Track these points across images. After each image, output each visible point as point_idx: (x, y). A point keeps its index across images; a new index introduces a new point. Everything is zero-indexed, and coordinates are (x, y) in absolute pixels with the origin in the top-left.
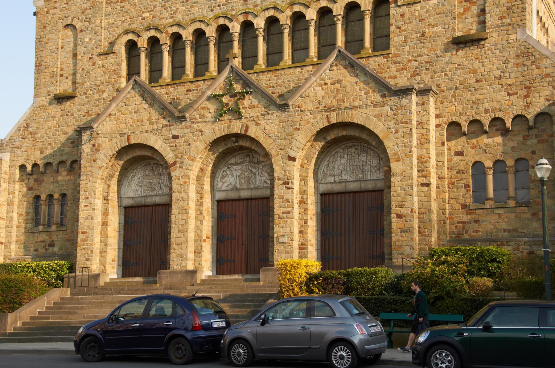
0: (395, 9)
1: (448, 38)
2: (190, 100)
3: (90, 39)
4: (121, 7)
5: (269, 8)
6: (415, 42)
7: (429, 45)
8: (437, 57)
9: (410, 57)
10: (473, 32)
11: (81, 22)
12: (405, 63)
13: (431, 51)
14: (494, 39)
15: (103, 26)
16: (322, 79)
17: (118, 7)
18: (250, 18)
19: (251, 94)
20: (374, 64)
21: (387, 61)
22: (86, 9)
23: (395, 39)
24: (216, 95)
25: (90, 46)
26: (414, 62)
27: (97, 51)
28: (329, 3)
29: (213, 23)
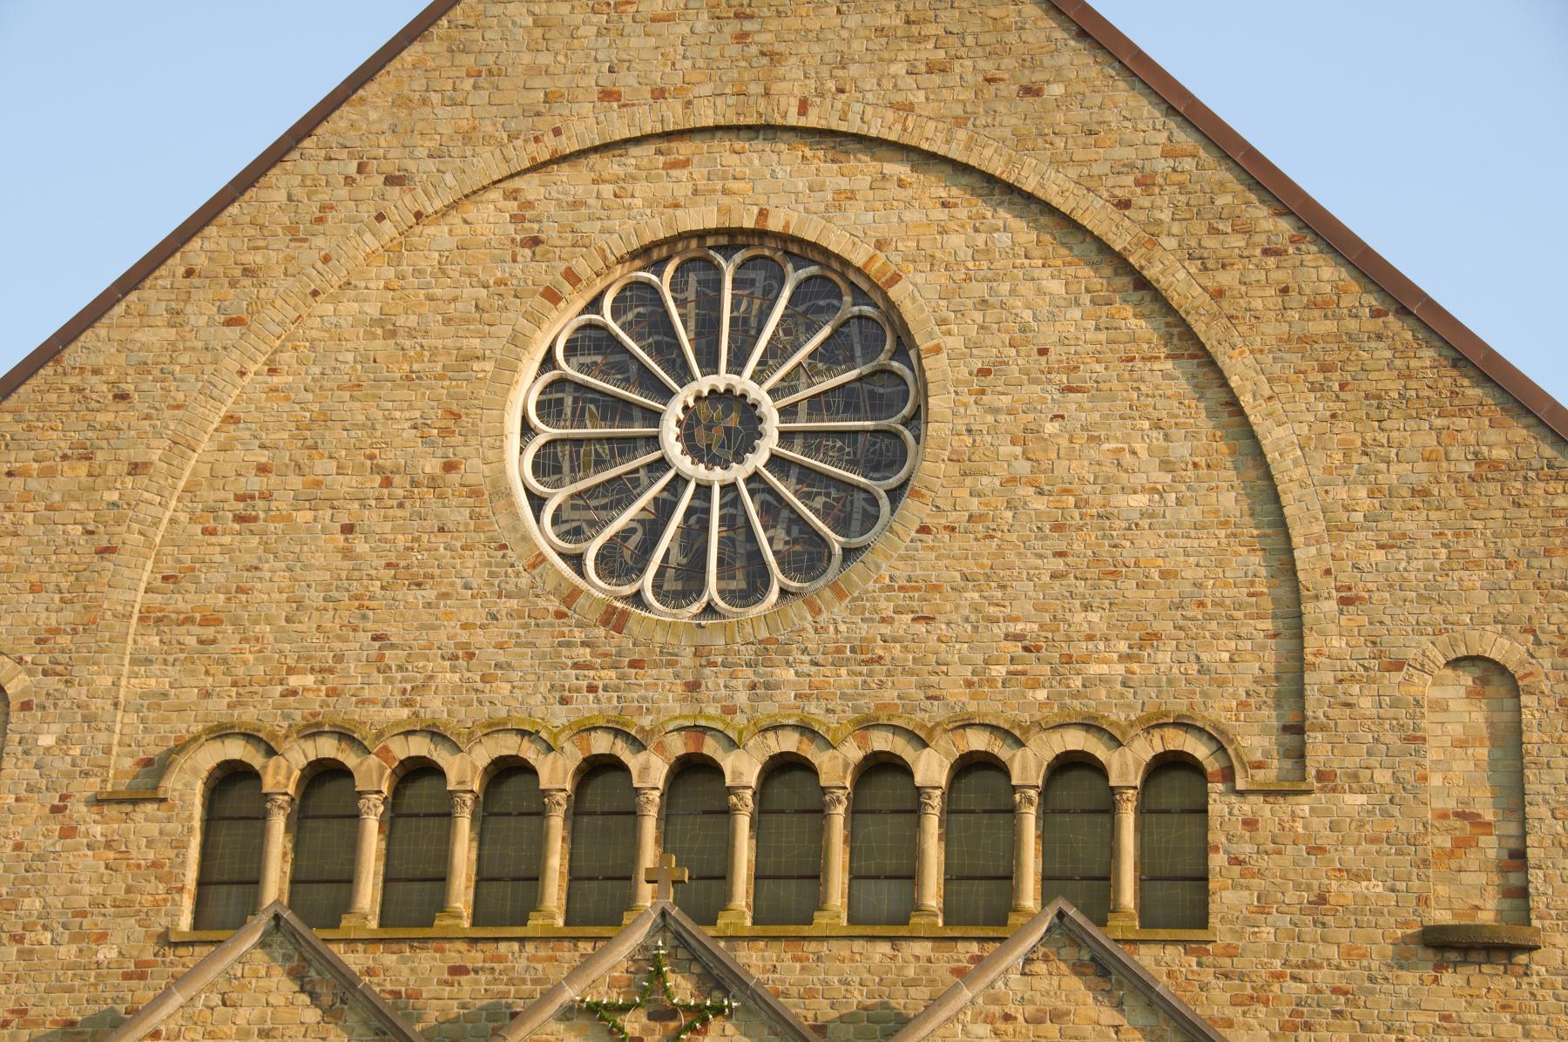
0: (1227, 799)
1: (1406, 924)
2: (463, 1006)
3: (63, 740)
4: (201, 642)
5: (783, 726)
6: (1296, 918)
7: (1343, 936)
8: (1371, 979)
9: (1277, 963)
10: (1487, 917)
11: (30, 673)
12: (1260, 982)
13: (1348, 954)
14: (1559, 952)
15: (122, 699)
16: (995, 1000)
17: (192, 641)
18: (711, 748)
19: (730, 1017)
20: (1159, 961)
21: (1199, 964)
22: (56, 631)
23: (1227, 899)
24: (598, 1004)
25: (61, 764)
26: (1293, 984)
27: (93, 785)
28: (999, 742)
29: (568, 746)
